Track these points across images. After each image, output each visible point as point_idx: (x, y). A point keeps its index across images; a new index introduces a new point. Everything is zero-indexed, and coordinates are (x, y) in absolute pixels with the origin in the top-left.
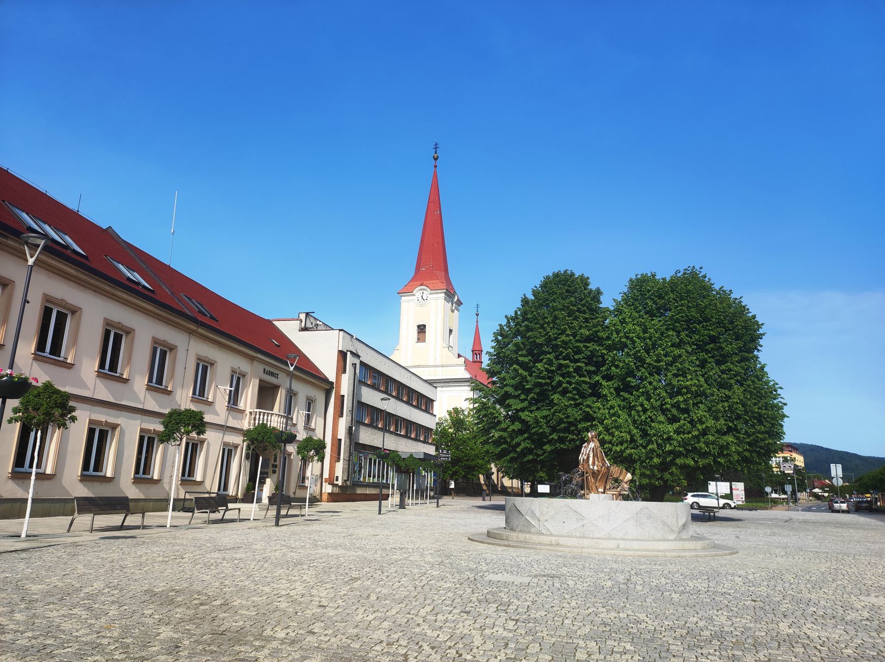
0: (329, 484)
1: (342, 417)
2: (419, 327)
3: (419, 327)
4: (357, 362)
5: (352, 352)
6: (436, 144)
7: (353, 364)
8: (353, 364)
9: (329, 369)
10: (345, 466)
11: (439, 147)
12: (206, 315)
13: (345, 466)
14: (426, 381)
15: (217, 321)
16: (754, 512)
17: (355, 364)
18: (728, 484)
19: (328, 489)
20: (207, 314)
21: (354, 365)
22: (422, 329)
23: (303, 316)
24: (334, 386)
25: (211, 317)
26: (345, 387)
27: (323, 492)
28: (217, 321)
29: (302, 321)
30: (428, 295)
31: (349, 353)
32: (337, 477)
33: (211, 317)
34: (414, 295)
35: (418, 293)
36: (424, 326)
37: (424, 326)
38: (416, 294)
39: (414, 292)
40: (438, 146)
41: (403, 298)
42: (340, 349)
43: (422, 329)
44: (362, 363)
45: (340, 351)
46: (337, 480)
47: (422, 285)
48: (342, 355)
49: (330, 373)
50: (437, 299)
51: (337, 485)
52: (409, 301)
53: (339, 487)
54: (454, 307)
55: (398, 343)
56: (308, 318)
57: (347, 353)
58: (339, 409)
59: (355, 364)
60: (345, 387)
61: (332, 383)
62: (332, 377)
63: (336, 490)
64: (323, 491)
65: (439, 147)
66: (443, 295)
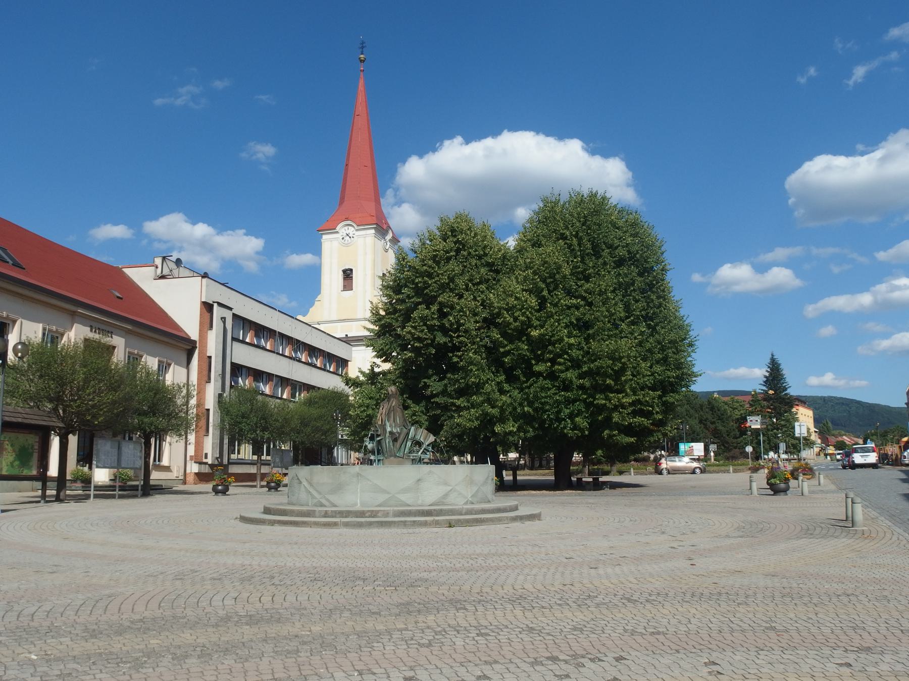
0: (195, 462)
1: (210, 382)
2: (344, 271)
3: (344, 271)
4: (228, 315)
5: (220, 304)
6: (363, 43)
7: (222, 318)
8: (222, 318)
9: (190, 325)
10: (216, 441)
11: (366, 46)
12: (8, 262)
13: (216, 441)
14: (338, 339)
15: (24, 269)
16: (529, 513)
17: (225, 318)
18: (41, 488)
19: (194, 468)
20: (8, 260)
21: (223, 319)
22: (348, 274)
23: (158, 261)
24: (198, 345)
25: (16, 265)
26: (213, 346)
27: (187, 472)
28: (24, 269)
29: (157, 267)
30: (355, 232)
31: (215, 305)
32: (206, 454)
33: (16, 265)
34: (337, 232)
35: (343, 230)
36: (351, 270)
37: (351, 270)
38: (340, 232)
39: (338, 228)
40: (364, 45)
41: (324, 237)
42: (203, 300)
43: (348, 274)
44: (235, 316)
45: (203, 302)
46: (206, 457)
47: (347, 219)
48: (208, 307)
49: (192, 330)
50: (365, 236)
51: (206, 463)
52: (331, 240)
53: (209, 465)
54: (388, 246)
55: (319, 293)
56: (165, 264)
57: (213, 305)
58: (205, 373)
59: (225, 318)
60: (213, 346)
61: (195, 342)
62: (194, 335)
63: (206, 469)
64: (188, 471)
65: (366, 46)
66: (373, 231)
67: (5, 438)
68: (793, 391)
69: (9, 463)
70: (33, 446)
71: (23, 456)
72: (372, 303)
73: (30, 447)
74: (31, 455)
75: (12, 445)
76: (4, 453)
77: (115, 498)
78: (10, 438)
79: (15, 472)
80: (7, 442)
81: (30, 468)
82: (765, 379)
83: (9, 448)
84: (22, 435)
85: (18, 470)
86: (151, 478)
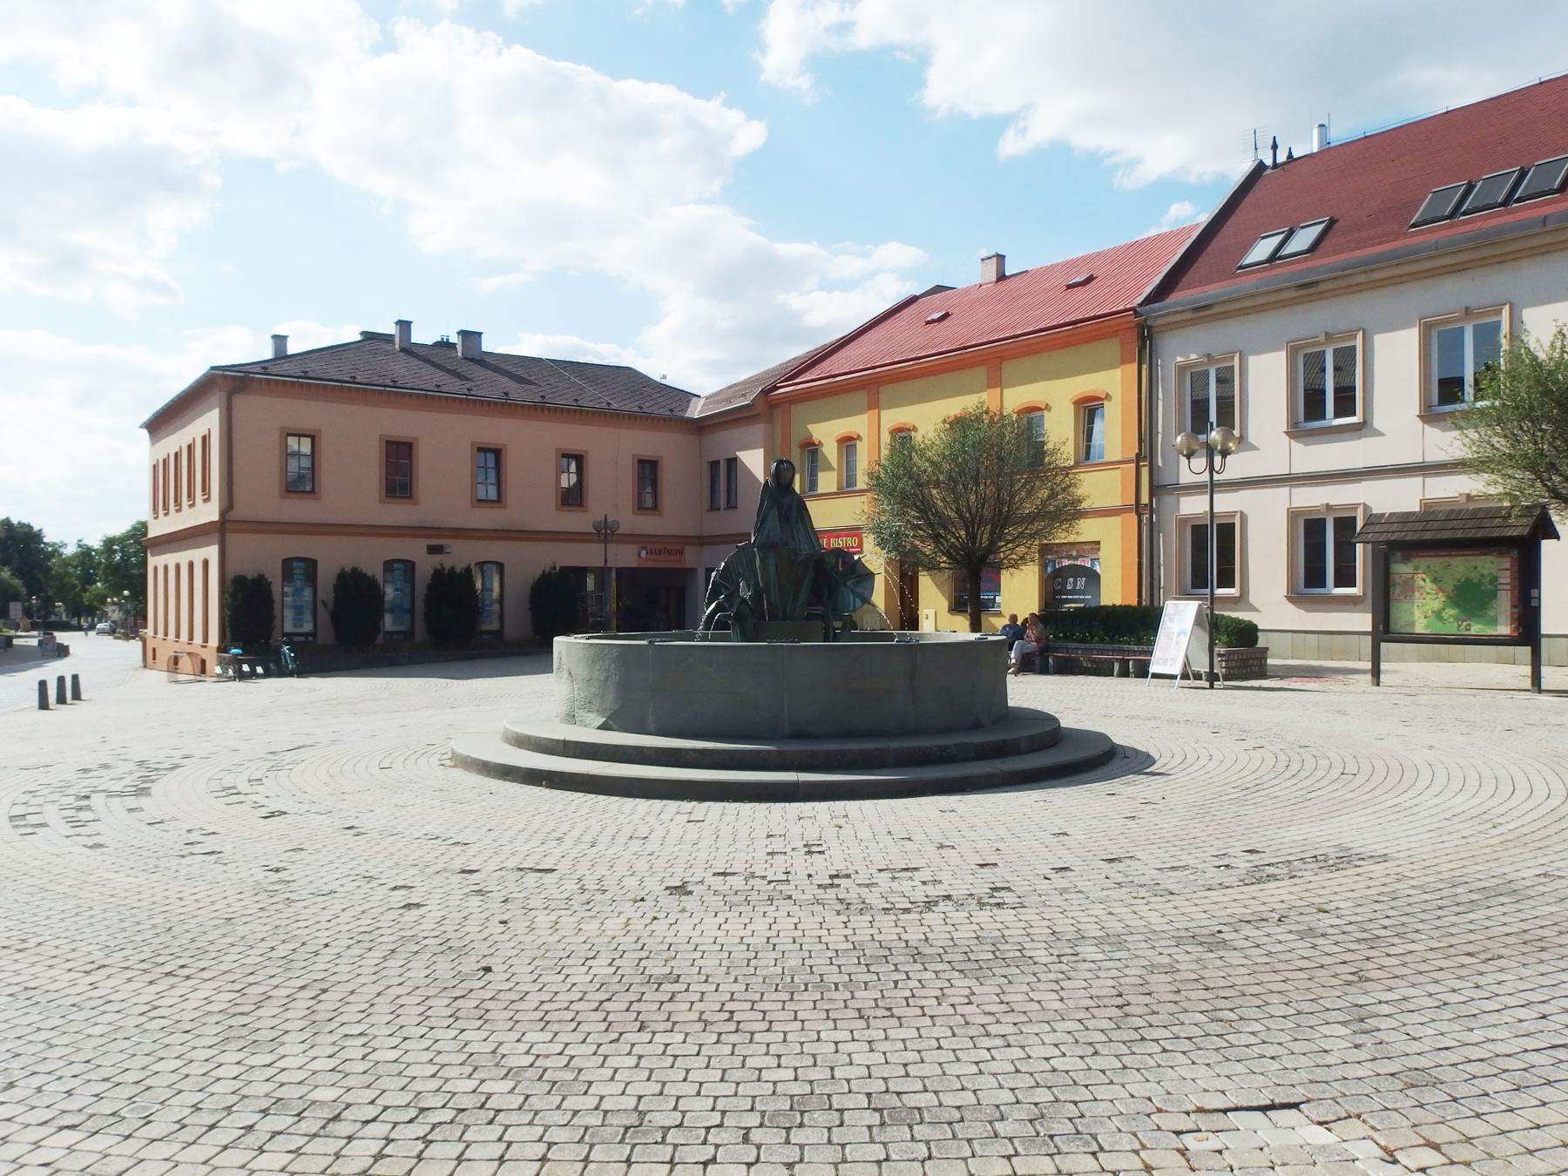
66: (45, 540)
67: (1417, 568)
68: (883, 412)
69: (1430, 613)
70: (1494, 580)
71: (1470, 598)
72: (499, 53)
73: (1486, 581)
74: (1493, 595)
75: (1435, 581)
76: (1417, 594)
77: (1110, 674)
78: (1429, 567)
79: (1451, 628)
80: (1424, 576)
81: (1494, 621)
82: (439, 567)
83: (1429, 586)
84: (1460, 559)
85: (1455, 625)
86: (1543, 631)
